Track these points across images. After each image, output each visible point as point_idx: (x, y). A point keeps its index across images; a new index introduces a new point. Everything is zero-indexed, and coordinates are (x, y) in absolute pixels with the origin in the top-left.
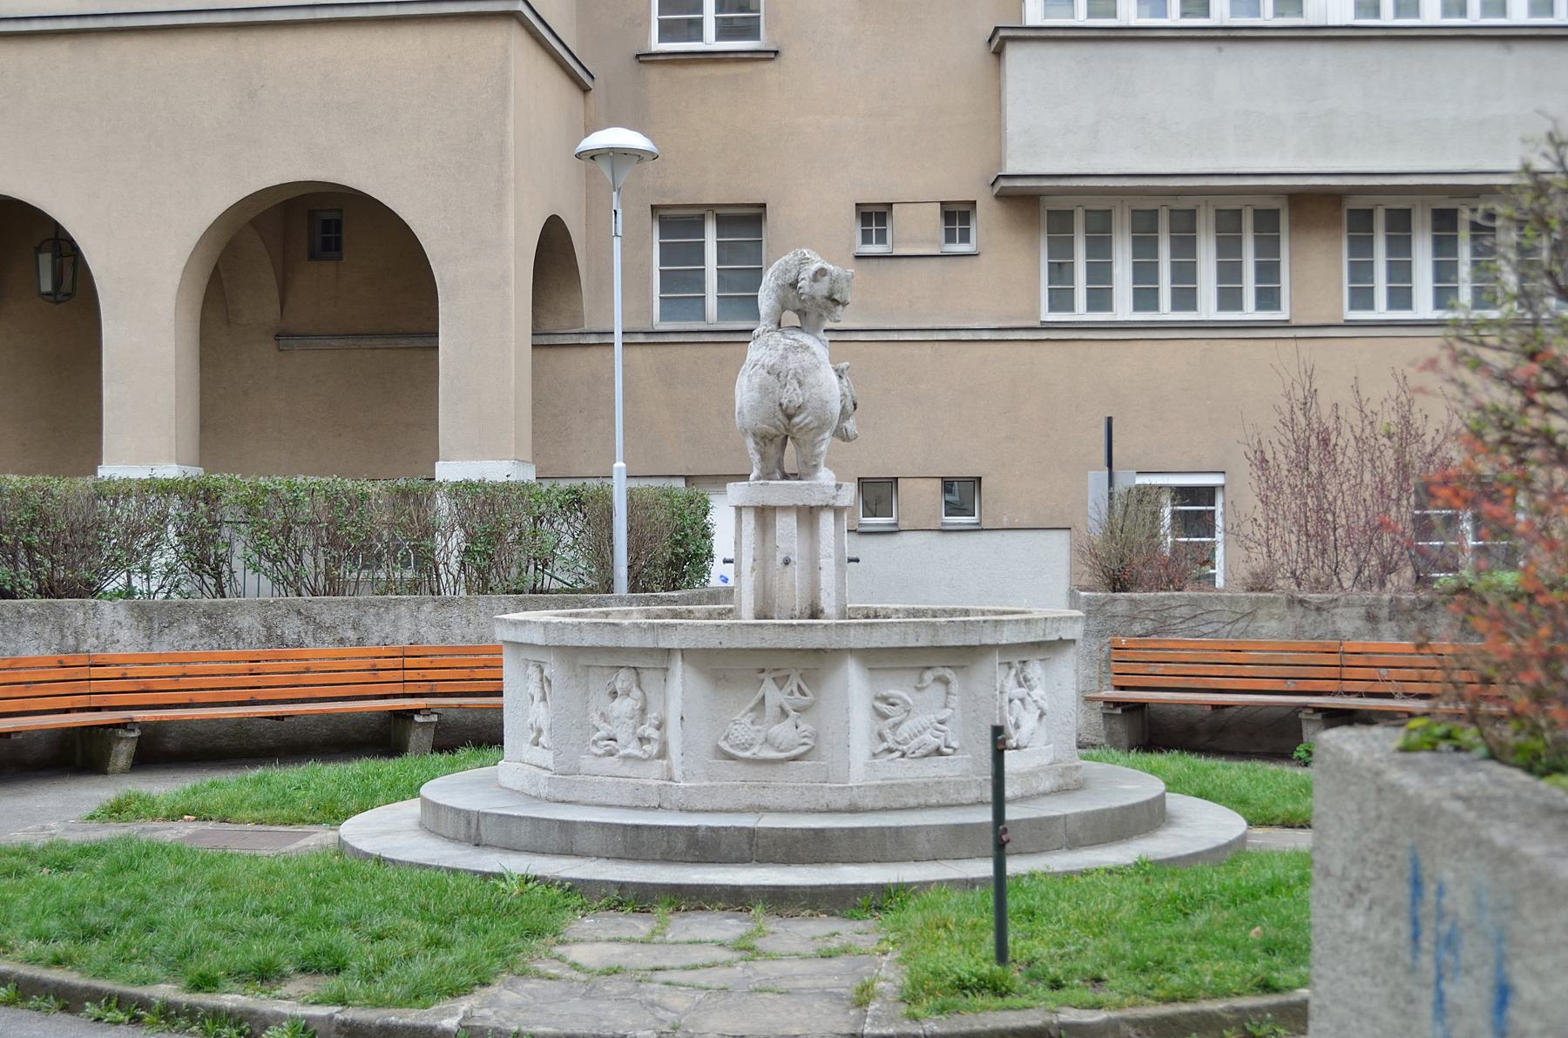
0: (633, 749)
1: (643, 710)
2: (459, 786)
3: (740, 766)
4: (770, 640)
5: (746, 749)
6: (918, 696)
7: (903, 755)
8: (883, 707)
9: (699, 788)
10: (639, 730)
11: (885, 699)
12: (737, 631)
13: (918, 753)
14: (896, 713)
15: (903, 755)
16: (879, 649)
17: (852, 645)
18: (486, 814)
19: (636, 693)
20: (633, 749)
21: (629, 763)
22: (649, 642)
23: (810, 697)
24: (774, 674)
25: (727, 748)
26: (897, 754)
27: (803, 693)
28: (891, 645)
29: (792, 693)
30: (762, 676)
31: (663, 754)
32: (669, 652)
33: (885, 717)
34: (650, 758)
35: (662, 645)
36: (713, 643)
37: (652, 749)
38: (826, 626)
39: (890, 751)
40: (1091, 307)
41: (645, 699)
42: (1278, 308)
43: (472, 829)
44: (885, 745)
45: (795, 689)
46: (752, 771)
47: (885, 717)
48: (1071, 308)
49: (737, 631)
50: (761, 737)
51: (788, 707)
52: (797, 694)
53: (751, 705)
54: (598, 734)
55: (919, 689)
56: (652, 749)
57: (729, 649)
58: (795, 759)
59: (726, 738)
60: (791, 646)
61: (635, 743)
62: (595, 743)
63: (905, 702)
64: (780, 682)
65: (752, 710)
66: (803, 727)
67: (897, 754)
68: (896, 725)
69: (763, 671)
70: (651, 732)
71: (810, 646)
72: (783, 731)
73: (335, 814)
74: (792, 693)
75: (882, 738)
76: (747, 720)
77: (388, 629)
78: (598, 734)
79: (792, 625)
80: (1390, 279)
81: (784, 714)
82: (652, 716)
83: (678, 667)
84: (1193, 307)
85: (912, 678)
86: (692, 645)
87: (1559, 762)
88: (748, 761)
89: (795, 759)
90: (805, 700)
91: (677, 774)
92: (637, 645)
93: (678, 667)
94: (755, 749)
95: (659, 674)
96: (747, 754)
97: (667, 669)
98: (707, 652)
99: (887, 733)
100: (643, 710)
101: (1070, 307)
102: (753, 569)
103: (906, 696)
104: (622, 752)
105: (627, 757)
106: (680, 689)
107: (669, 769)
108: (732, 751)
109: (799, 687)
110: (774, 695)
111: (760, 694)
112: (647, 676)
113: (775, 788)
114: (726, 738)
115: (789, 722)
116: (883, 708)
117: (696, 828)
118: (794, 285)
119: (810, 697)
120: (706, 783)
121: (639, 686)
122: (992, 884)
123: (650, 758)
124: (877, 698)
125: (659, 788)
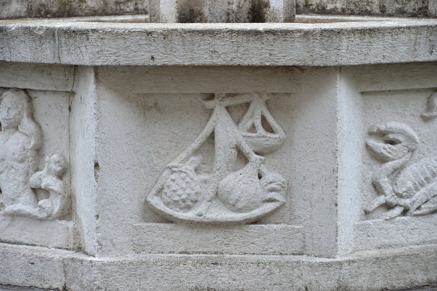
0: (25, 204)
1: (39, 151)
3: (178, 232)
4: (201, 55)
5: (188, 208)
6: (425, 129)
7: (405, 212)
8: (379, 146)
9: (121, 265)
10: (34, 179)
11: (381, 135)
12: (176, 40)
13: (425, 209)
14: (396, 154)
15: (405, 212)
16: (378, 66)
17: (344, 62)
19: (27, 125)
20: (25, 204)
21: (20, 223)
22: (47, 56)
23: (280, 134)
24: (228, 102)
25: (158, 203)
26: (398, 211)
27: (269, 129)
28: (396, 59)
29: (253, 128)
30: (210, 104)
31: (68, 212)
32: (75, 70)
33: (381, 159)
34: (49, 218)
35: (68, 59)
36: (141, 58)
37: (53, 205)
38: (307, 33)
39: (388, 206)
41: (41, 135)
44: (382, 199)
45: (258, 123)
46: (196, 239)
47: (381, 159)
49: (176, 40)
50: (211, 192)
51: (247, 149)
52: (261, 130)
53: (195, 145)
55: (426, 119)
57: (164, 67)
58: (257, 221)
59: (159, 192)
60: (256, 62)
61: (27, 196)
63: (410, 138)
64: (238, 111)
65: (196, 152)
66: (269, 176)
67: (398, 211)
68: (397, 171)
69: (211, 97)
70: (49, 181)
71: (282, 62)
72: (241, 183)
74: (253, 128)
75: (377, 188)
76: (189, 167)
79: (257, 33)
81: (242, 158)
82: (52, 160)
83: (89, 91)
85: (418, 103)
86: (111, 61)
88: (191, 224)
89: (257, 221)
90: (272, 139)
91: (90, 243)
92: (412, 60)
93: (89, 91)
94: (201, 208)
95: (62, 101)
96: (190, 215)
97: (73, 93)
98: (132, 70)
99: (385, 182)
100: (39, 151)
103: (409, 130)
106: (94, 123)
107: (77, 234)
108: (168, 210)
109: (264, 120)
110: (228, 132)
111: (207, 131)
112: (43, 103)
113: (232, 264)
114: (159, 192)
115: (249, 170)
116: (380, 145)
119: (280, 134)
120: (131, 257)
121: (32, 116)
122: (57, 61)
123: (49, 218)
124: (371, 134)
125: (65, 264)
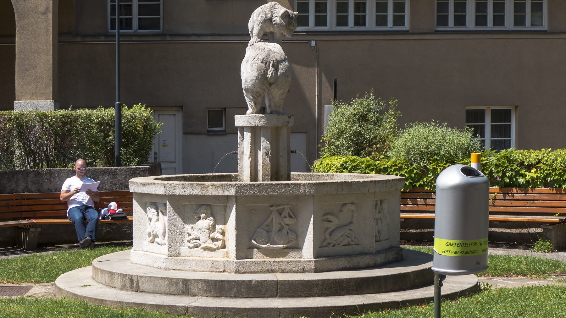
0: (210, 244)
2: (114, 260)
10: (212, 235)
18: (142, 277)
31: (224, 247)
34: (218, 248)
37: (219, 244)
40: (495, 24)
42: (326, 25)
43: (133, 283)
48: (386, 24)
54: (191, 237)
56: (219, 244)
61: (210, 241)
62: (189, 241)
73: (50, 276)
77: (14, 186)
78: (191, 237)
80: (316, 11)
84: (325, 25)
87: (287, 216)
101: (485, 24)
102: (250, 157)
104: (203, 245)
105: (206, 249)
107: (227, 253)
117: (251, 281)
118: (270, 19)
123: (218, 248)
